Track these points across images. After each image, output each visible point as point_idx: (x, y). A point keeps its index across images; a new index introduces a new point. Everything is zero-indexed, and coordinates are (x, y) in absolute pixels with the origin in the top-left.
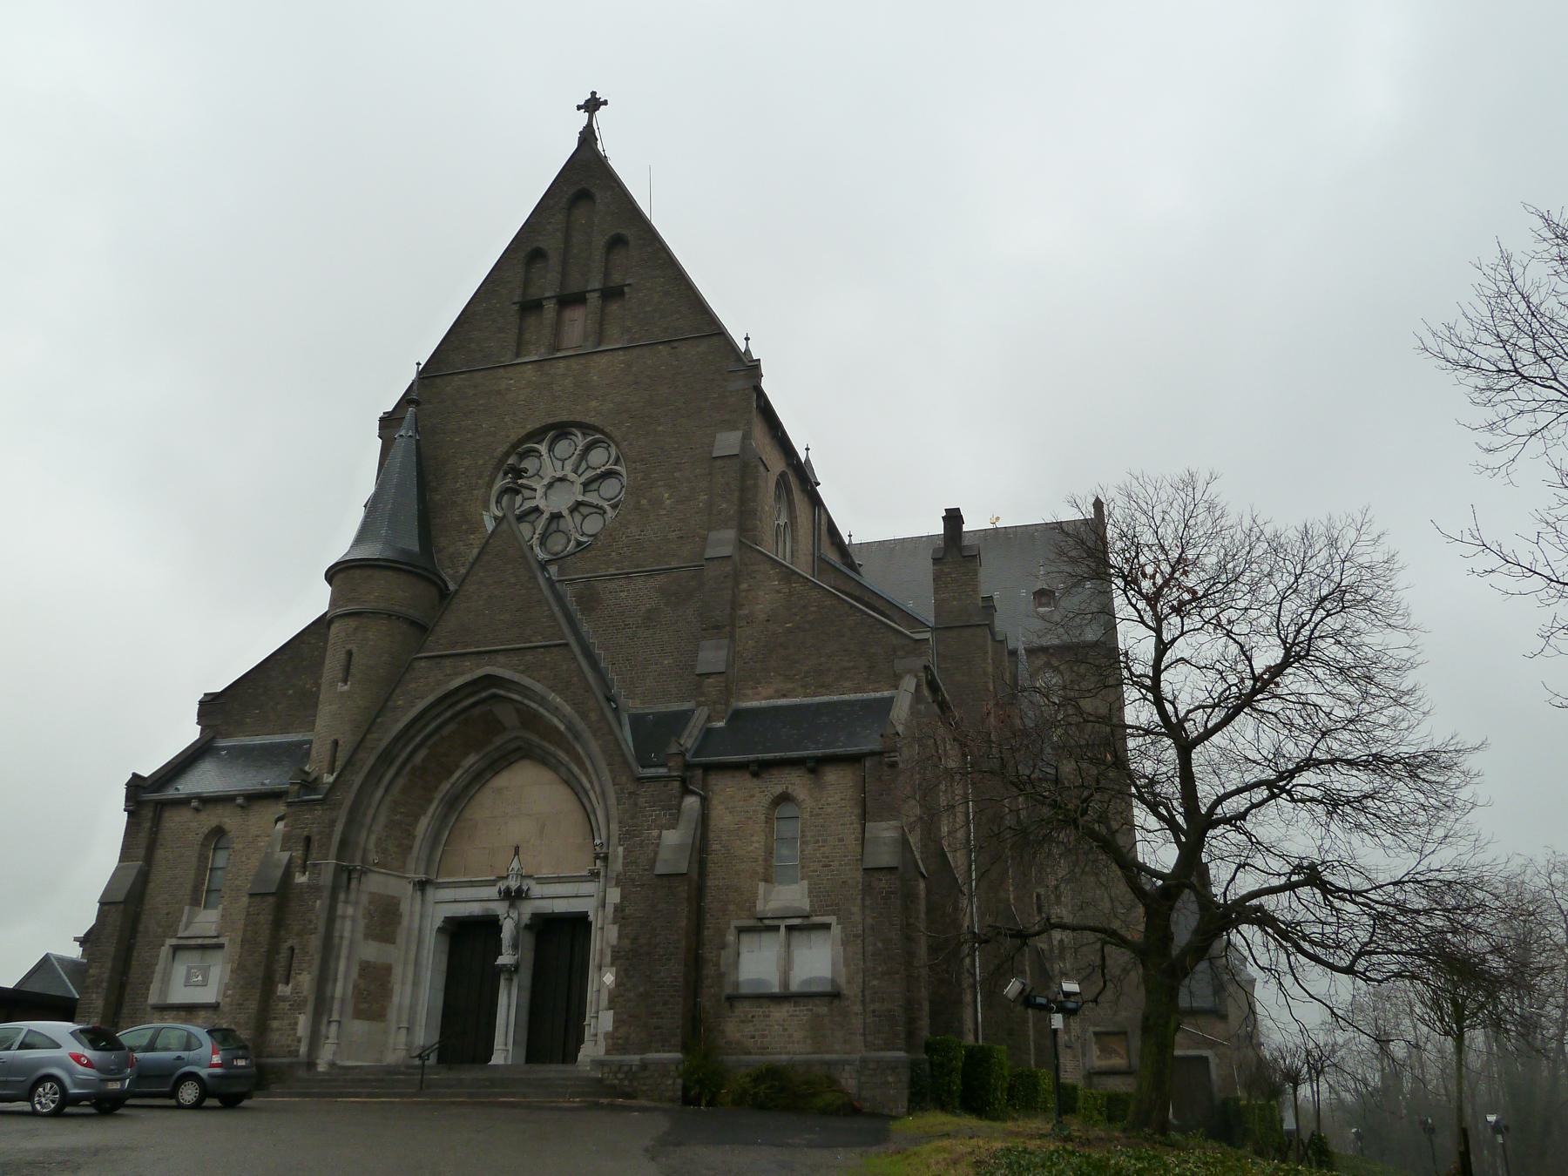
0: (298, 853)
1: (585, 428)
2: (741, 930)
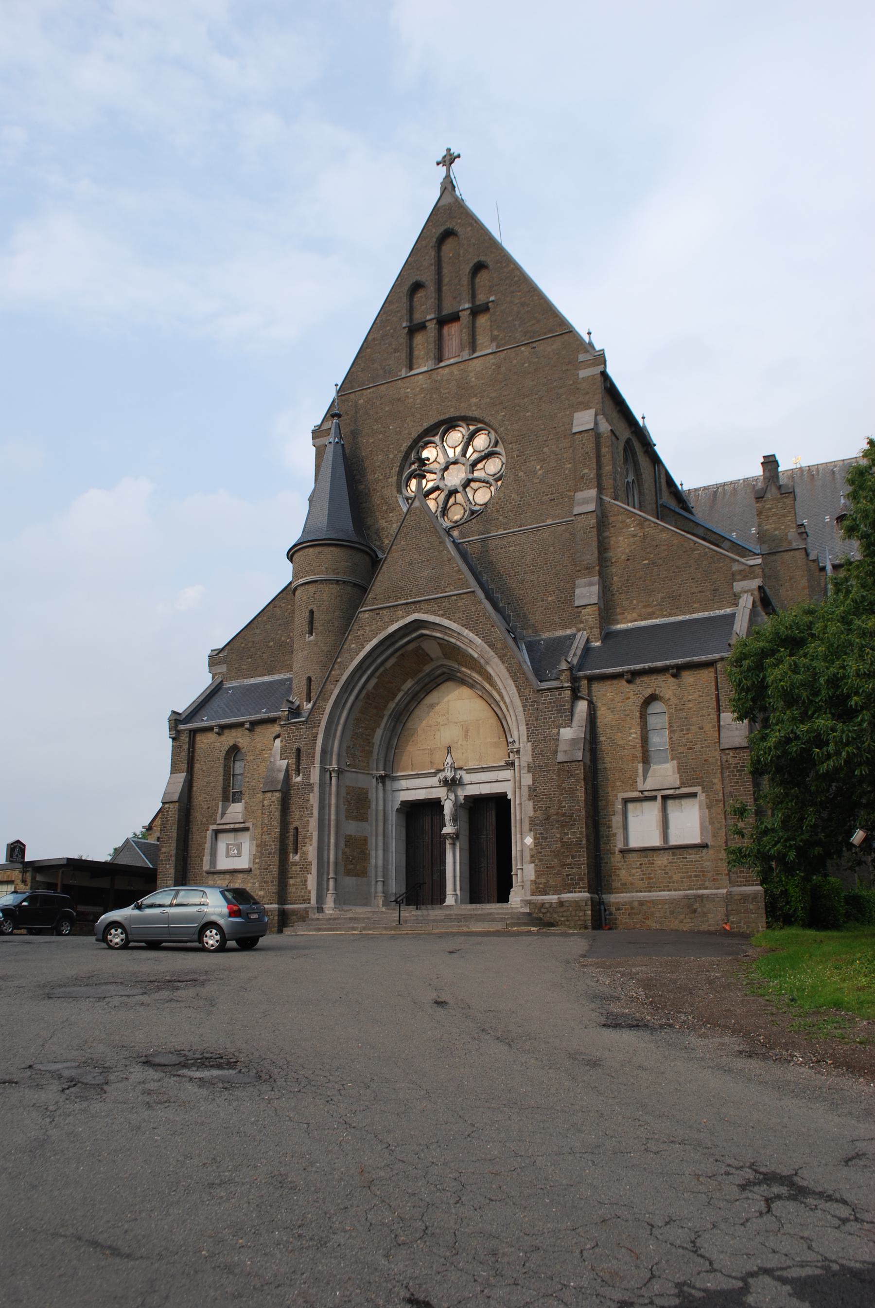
0: (293, 761)
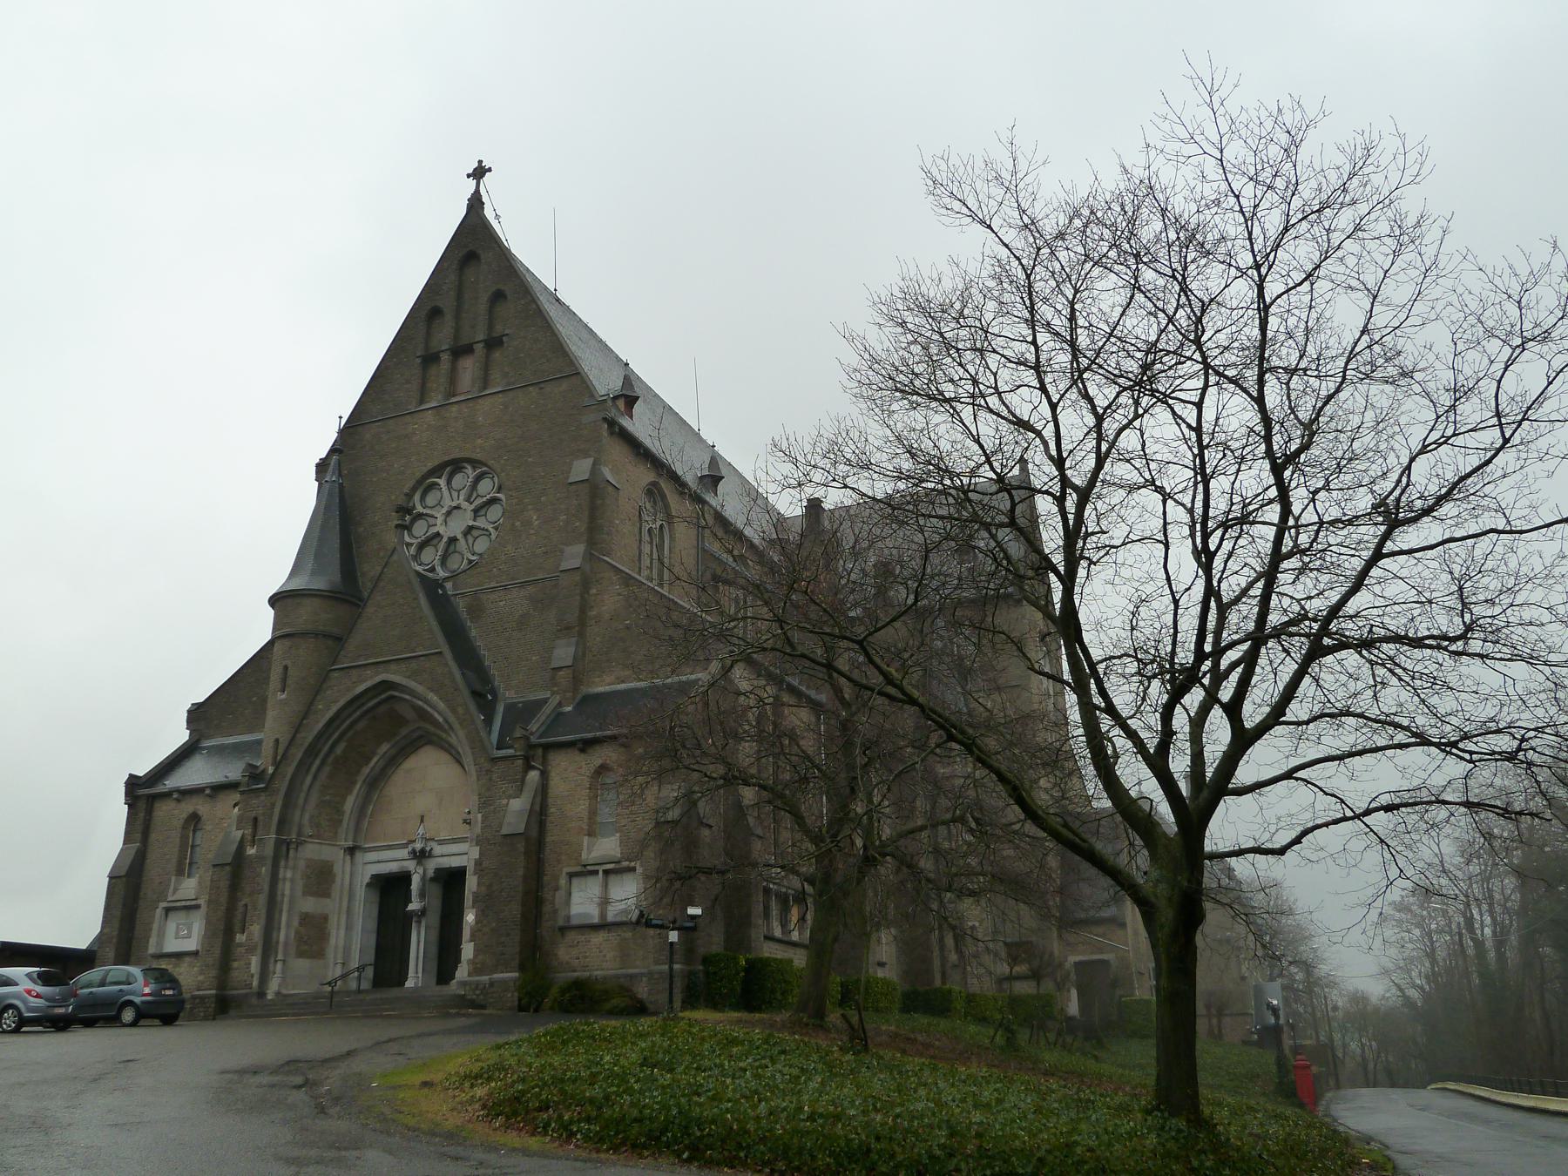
0: (248, 831)
1: (475, 463)
2: (571, 875)
